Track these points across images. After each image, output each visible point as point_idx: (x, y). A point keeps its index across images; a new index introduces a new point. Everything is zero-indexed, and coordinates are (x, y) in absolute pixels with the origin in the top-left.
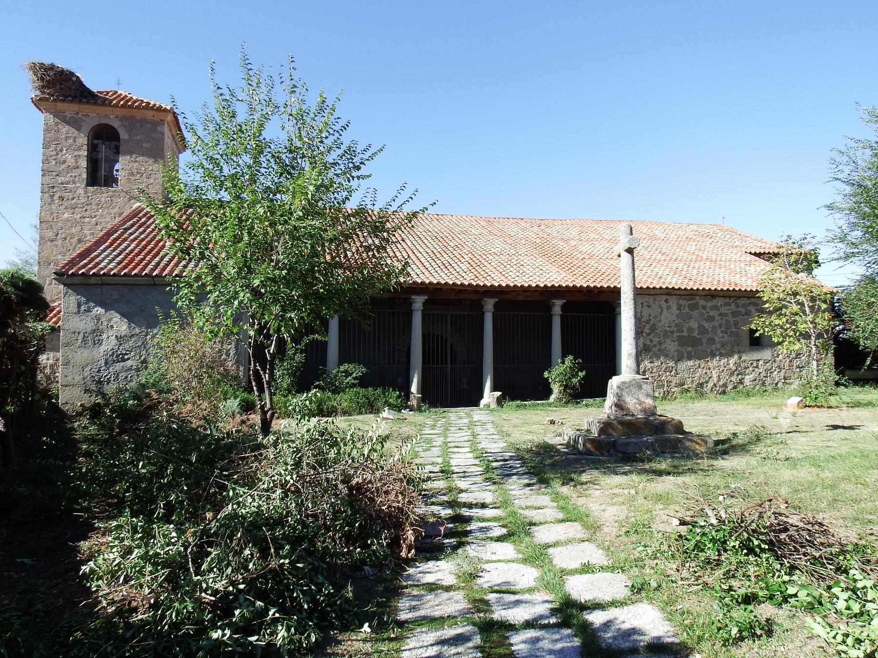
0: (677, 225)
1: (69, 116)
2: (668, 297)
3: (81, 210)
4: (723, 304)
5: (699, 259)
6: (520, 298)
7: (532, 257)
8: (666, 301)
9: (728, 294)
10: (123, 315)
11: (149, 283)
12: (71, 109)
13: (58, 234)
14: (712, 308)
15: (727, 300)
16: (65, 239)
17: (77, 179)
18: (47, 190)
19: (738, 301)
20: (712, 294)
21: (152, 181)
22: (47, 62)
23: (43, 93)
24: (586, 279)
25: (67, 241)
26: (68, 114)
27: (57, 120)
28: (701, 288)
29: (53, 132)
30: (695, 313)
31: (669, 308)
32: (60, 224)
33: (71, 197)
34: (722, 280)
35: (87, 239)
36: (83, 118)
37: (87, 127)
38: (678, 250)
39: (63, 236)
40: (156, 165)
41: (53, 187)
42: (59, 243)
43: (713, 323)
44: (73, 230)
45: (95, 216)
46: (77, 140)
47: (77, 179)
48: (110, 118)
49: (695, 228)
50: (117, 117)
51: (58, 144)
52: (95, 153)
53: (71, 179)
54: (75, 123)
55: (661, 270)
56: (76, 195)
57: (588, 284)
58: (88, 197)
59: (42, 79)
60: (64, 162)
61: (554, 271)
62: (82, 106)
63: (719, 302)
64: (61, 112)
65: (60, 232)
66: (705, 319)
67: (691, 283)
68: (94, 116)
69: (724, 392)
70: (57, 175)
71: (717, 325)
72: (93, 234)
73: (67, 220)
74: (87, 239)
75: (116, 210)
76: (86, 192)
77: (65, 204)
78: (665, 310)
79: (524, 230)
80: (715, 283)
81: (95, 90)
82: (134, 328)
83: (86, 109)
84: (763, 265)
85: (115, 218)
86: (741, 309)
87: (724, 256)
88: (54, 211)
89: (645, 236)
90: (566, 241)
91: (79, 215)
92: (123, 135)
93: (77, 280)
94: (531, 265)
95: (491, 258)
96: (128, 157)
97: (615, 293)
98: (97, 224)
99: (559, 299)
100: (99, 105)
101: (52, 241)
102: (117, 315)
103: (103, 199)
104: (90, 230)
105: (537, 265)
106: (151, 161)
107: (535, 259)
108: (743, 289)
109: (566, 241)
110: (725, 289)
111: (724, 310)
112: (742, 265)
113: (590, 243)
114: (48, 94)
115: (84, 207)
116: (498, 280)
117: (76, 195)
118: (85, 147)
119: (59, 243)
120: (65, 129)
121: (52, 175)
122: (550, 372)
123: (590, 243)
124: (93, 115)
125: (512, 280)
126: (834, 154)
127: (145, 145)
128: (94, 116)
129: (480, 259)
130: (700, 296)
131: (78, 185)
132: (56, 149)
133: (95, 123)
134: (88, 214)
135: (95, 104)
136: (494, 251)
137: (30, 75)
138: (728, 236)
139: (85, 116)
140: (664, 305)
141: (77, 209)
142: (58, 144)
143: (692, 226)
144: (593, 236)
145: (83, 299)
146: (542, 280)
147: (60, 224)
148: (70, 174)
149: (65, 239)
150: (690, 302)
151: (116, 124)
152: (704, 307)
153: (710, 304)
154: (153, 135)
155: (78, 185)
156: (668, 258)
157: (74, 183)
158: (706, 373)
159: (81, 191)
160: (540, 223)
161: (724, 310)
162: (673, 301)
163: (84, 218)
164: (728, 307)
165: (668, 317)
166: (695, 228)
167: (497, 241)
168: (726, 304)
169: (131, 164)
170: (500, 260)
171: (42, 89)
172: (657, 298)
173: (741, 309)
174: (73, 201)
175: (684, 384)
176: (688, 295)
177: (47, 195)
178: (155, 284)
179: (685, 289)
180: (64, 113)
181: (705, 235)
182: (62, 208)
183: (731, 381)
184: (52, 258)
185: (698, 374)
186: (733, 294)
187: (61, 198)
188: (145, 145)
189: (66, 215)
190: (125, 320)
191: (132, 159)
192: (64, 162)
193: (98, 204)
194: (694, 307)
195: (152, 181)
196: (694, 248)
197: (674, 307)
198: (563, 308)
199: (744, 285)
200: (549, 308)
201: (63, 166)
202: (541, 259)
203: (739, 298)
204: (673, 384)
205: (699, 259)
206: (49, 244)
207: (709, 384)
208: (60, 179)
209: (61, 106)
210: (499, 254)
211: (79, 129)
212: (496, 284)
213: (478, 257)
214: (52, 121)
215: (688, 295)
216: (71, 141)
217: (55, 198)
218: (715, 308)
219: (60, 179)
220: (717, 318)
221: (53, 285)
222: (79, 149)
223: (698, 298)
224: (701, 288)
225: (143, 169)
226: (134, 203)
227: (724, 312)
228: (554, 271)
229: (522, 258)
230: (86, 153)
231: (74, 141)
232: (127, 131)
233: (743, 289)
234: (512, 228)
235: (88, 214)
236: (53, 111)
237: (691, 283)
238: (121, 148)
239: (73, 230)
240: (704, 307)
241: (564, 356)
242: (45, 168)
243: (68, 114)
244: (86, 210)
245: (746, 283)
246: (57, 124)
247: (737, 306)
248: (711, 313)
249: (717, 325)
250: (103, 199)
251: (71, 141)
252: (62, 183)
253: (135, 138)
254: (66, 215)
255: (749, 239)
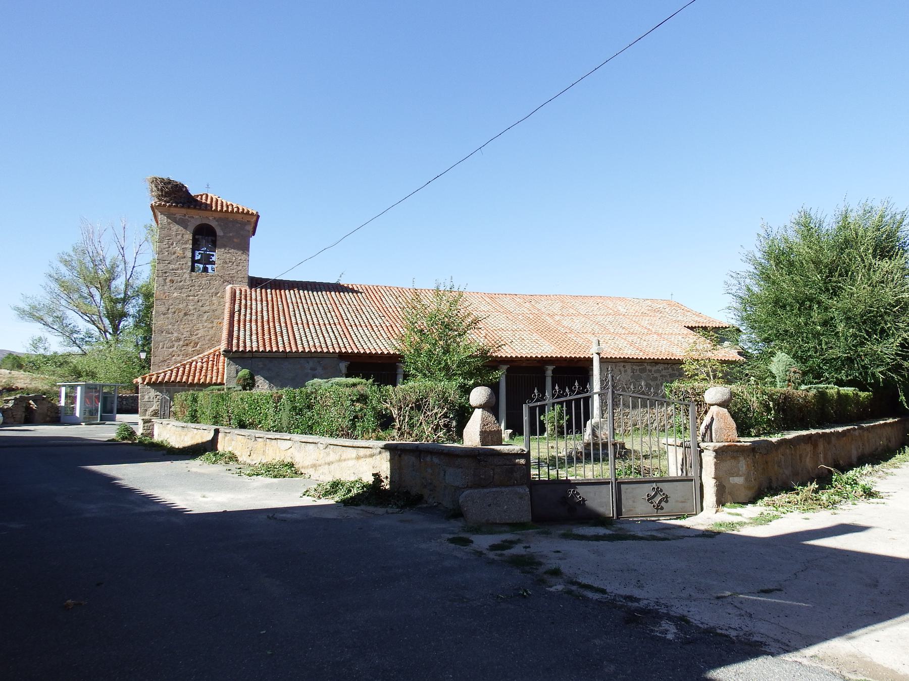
0: (635, 300)
1: (179, 217)
2: (626, 364)
3: (187, 290)
4: (663, 368)
5: (650, 332)
6: (524, 365)
7: (529, 332)
8: (624, 366)
9: (666, 361)
10: (266, 378)
11: (284, 357)
12: (180, 212)
13: (169, 309)
14: (656, 371)
15: (666, 366)
16: (175, 312)
17: (184, 267)
18: (161, 274)
19: (674, 366)
20: (655, 362)
21: (240, 268)
22: (165, 177)
23: (160, 200)
24: (569, 351)
25: (176, 314)
26: (178, 216)
27: (169, 220)
28: (647, 358)
29: (166, 229)
30: (644, 375)
31: (625, 371)
32: (171, 301)
33: (179, 280)
34: (663, 351)
35: (190, 313)
36: (189, 219)
37: (192, 227)
38: (634, 325)
39: (173, 310)
40: (244, 256)
41: (165, 273)
42: (170, 316)
43: (656, 382)
44: (181, 306)
45: (197, 295)
46: (184, 236)
47: (184, 267)
48: (209, 219)
49: (650, 303)
50: (215, 218)
51: (170, 239)
52: (196, 246)
53: (179, 266)
54: (183, 223)
55: (622, 343)
56: (183, 279)
57: (570, 355)
58: (192, 280)
59: (162, 191)
60: (175, 253)
61: (546, 345)
62: (189, 210)
63: (661, 367)
64: (173, 214)
65: (171, 307)
66: (651, 379)
67: (641, 354)
68: (197, 218)
69: (664, 431)
70: (169, 263)
71: (659, 383)
72: (195, 309)
73: (176, 298)
74: (190, 313)
75: (213, 291)
76: (191, 277)
77: (175, 285)
78: (623, 373)
79: (520, 305)
80: (658, 353)
81: (193, 193)
82: (273, 387)
83: (192, 212)
84: (692, 337)
85: (212, 296)
86: (676, 372)
87: (668, 329)
88: (166, 291)
89: (611, 311)
90: (551, 316)
91: (186, 295)
92: (219, 232)
93: (237, 355)
94: (529, 339)
95: (500, 333)
96: (223, 250)
97: (590, 361)
98: (198, 301)
99: (550, 365)
100: (203, 210)
101: (164, 314)
102: (262, 378)
103: (203, 282)
104: (194, 305)
105: (534, 339)
106: (240, 253)
107: (531, 334)
108: (677, 359)
109: (551, 316)
110: (664, 358)
111: (664, 373)
112: (680, 337)
113: (570, 318)
114: (165, 201)
115: (189, 288)
116: (509, 352)
117: (183, 279)
118: (191, 242)
119: (170, 316)
120: (175, 227)
121: (165, 263)
122: (544, 416)
123: (570, 318)
124: (197, 217)
125: (519, 352)
126: (728, 279)
127: (235, 240)
128: (197, 218)
129: (493, 334)
130: (647, 363)
131: (185, 271)
132: (168, 243)
133: (198, 223)
134: (192, 293)
135: (200, 209)
136: (501, 326)
137: (147, 186)
138: (674, 311)
139: (190, 217)
140: (623, 369)
141: (183, 290)
142: (170, 239)
143: (647, 301)
144: (571, 311)
145: (240, 367)
146: (539, 352)
147: (171, 301)
148: (179, 263)
149: (175, 312)
150: (640, 367)
151: (214, 224)
152: (650, 371)
153: (654, 368)
154: (242, 232)
155: (185, 271)
156: (627, 332)
157: (182, 269)
158: (652, 417)
159: (187, 276)
160: (531, 298)
161: (664, 373)
162: (629, 367)
163: (189, 296)
164: (667, 371)
165: (624, 377)
166: (650, 303)
167: (501, 317)
168: (665, 369)
169: (225, 255)
170: (507, 335)
171: (159, 197)
172: (618, 364)
173: (676, 372)
174: (181, 284)
175: (636, 425)
176: (639, 363)
177: (161, 278)
178: (286, 358)
179: (637, 358)
180: (175, 215)
181: (656, 310)
182: (172, 288)
183: (669, 423)
184: (164, 328)
185: (646, 418)
186: (670, 362)
187: (172, 281)
188: (235, 240)
189: (175, 295)
190: (267, 382)
191: (226, 251)
192: (175, 253)
193: (199, 286)
194: (643, 371)
195: (240, 268)
196: (647, 322)
197: (629, 371)
198: (553, 371)
199: (678, 355)
200: (543, 372)
201: (174, 256)
202: (536, 334)
203: (675, 364)
204: (629, 425)
205: (650, 332)
206: (162, 316)
207: (653, 425)
208: (171, 266)
209: (173, 210)
210: (505, 329)
211: (186, 228)
212: (509, 356)
213: (491, 332)
214: (166, 221)
215: (639, 363)
216: (179, 237)
217: (167, 281)
218: (658, 371)
219: (171, 266)
220: (659, 378)
221: (165, 349)
222: (186, 243)
223: (646, 364)
224: (647, 358)
225: (234, 258)
226: (227, 285)
227: (664, 374)
228: (546, 345)
229: (522, 333)
230: (191, 246)
231: (182, 237)
232: (222, 229)
233: (677, 359)
234: (509, 304)
235: (192, 293)
236: (166, 213)
237: (641, 354)
238: (218, 243)
239: (181, 306)
240: (650, 371)
241: (725, 593)
242: (160, 258)
243: (178, 216)
244: (191, 290)
245: (678, 353)
246: (169, 224)
247: (673, 370)
248: (655, 375)
249: (659, 383)
250: (203, 282)
251: (179, 237)
252: (173, 270)
253: (228, 235)
254: (175, 295)
255: (689, 313)
